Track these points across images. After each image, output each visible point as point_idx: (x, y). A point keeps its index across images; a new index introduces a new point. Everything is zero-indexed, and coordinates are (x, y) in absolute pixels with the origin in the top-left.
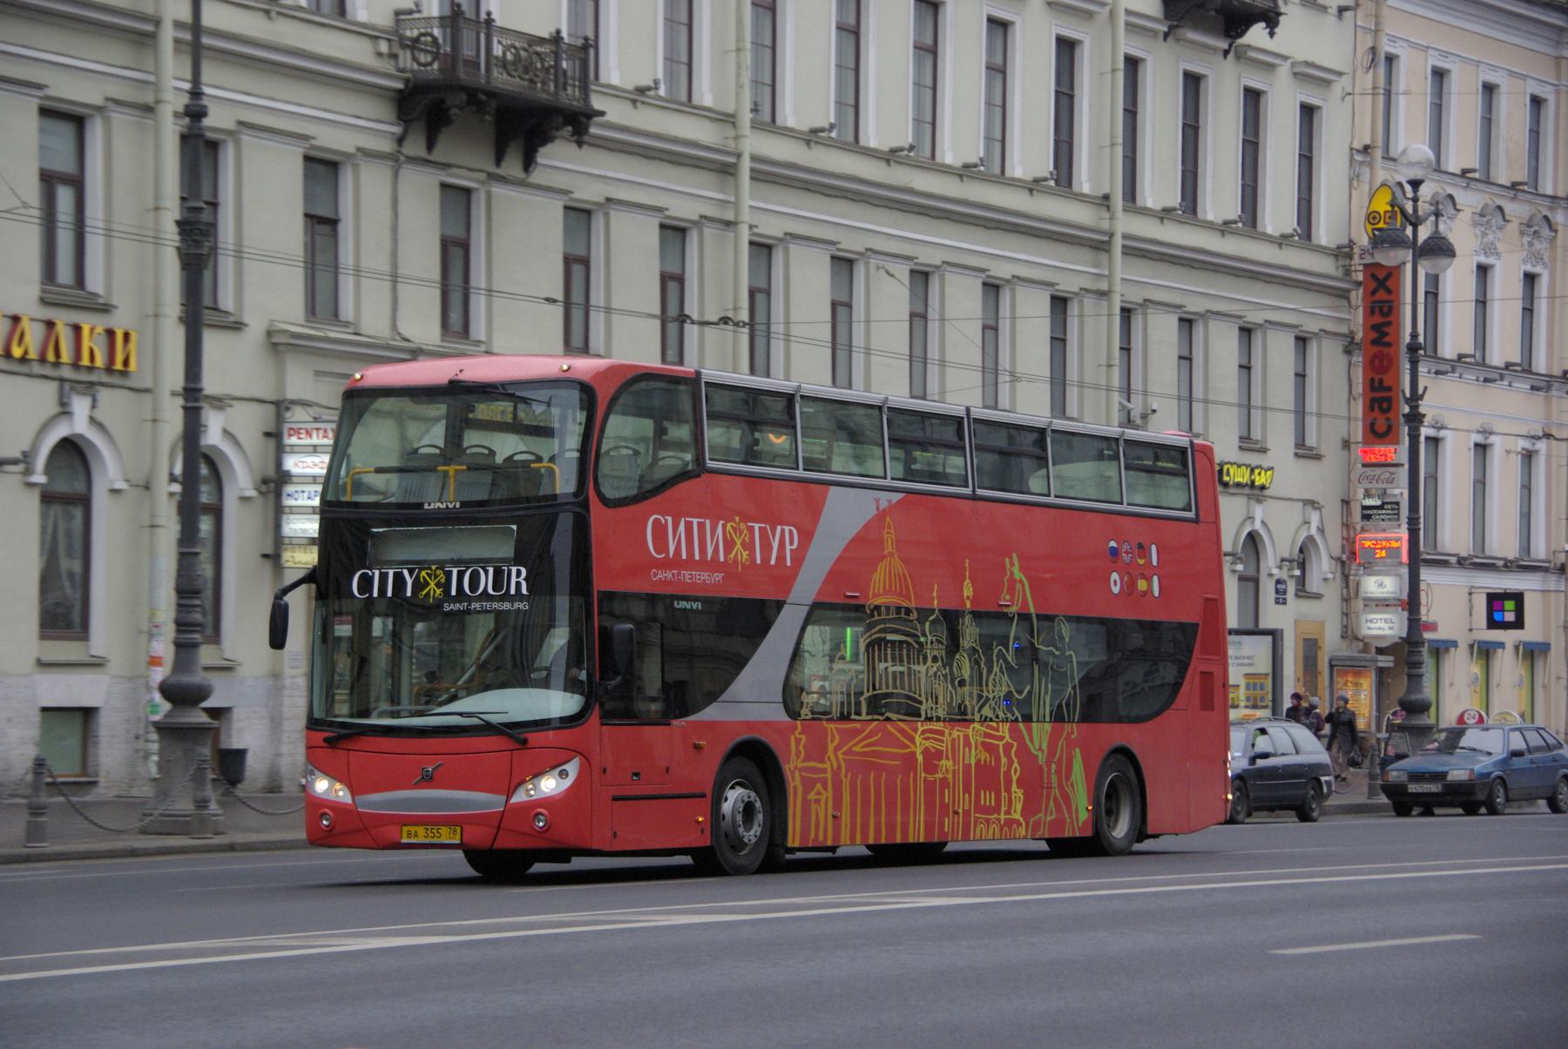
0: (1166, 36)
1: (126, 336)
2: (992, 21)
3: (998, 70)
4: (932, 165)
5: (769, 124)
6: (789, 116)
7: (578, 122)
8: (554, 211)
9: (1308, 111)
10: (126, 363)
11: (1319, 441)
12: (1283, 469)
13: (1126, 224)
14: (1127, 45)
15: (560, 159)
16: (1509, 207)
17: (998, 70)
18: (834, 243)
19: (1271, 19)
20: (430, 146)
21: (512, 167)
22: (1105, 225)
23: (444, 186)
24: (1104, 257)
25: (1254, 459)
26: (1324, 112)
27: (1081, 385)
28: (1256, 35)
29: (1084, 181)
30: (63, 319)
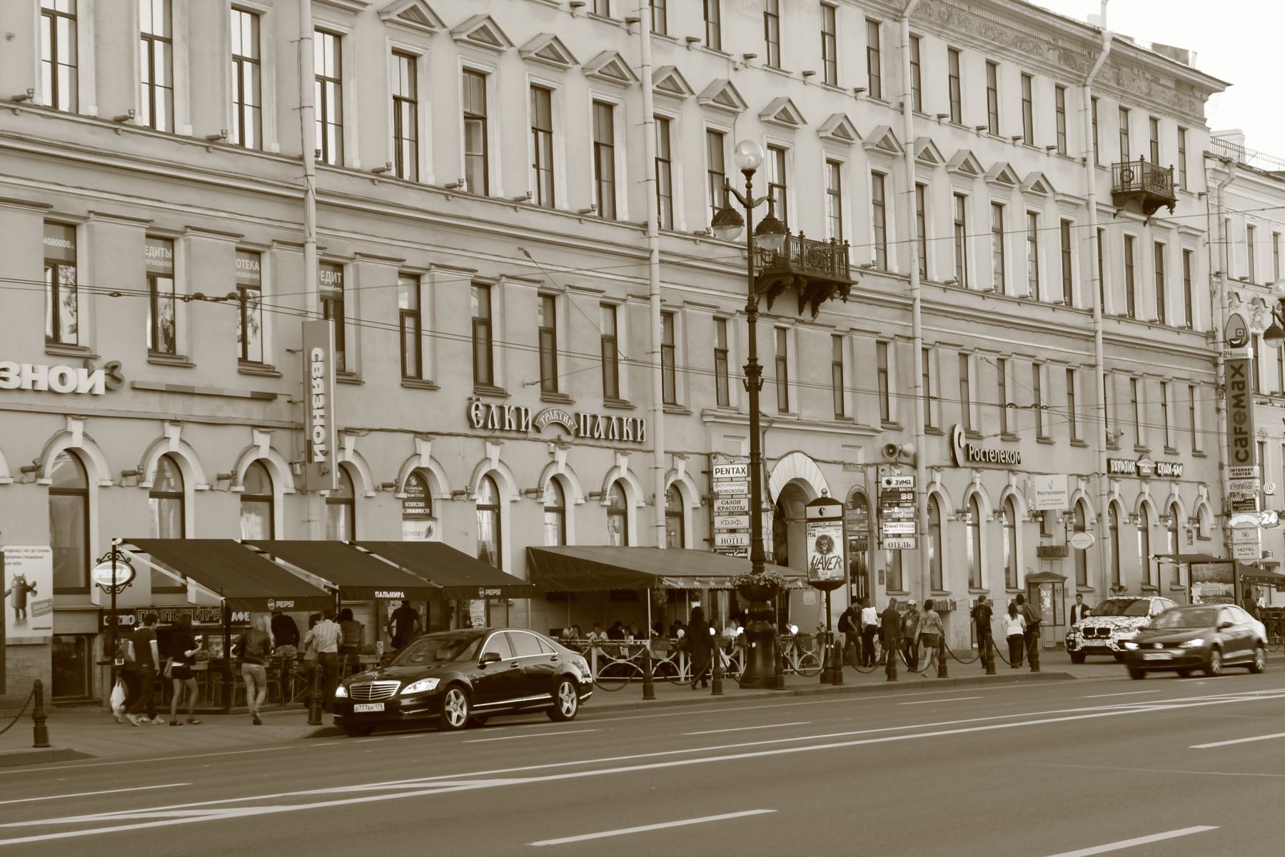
0: (1115, 215)
1: (526, 411)
2: (874, 173)
3: (543, 129)
4: (967, 290)
5: (669, 228)
6: (681, 224)
7: (844, 289)
8: (826, 334)
9: (1187, 253)
10: (642, 437)
11: (1176, 443)
12: (1187, 466)
13: (1101, 326)
14: (1096, 220)
15: (832, 309)
16: (1266, 298)
17: (543, 129)
18: (473, 271)
19: (1171, 203)
20: (769, 307)
21: (807, 315)
22: (1091, 326)
23: (776, 327)
24: (1091, 345)
25: (1172, 459)
26: (677, 120)
27: (854, 390)
28: (1162, 212)
29: (1078, 302)
30: (614, 415)
